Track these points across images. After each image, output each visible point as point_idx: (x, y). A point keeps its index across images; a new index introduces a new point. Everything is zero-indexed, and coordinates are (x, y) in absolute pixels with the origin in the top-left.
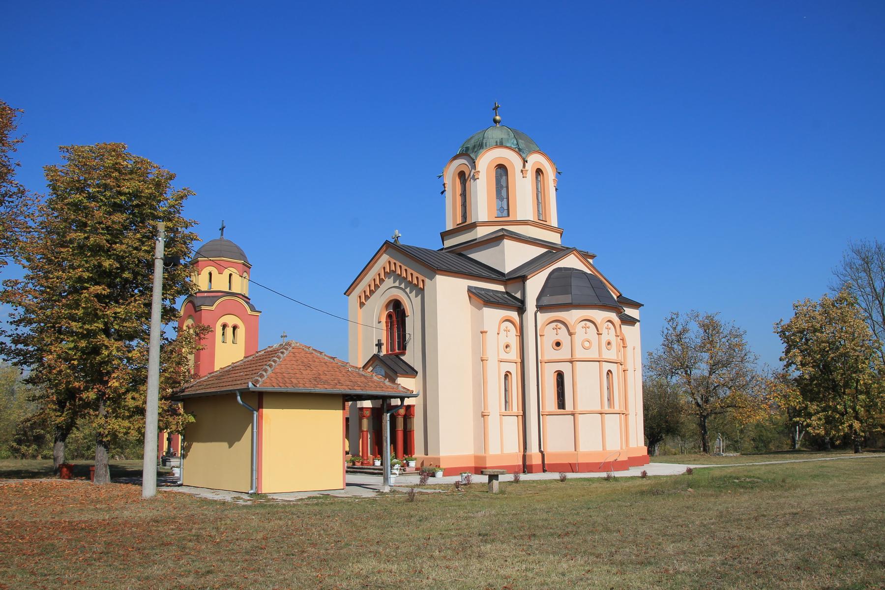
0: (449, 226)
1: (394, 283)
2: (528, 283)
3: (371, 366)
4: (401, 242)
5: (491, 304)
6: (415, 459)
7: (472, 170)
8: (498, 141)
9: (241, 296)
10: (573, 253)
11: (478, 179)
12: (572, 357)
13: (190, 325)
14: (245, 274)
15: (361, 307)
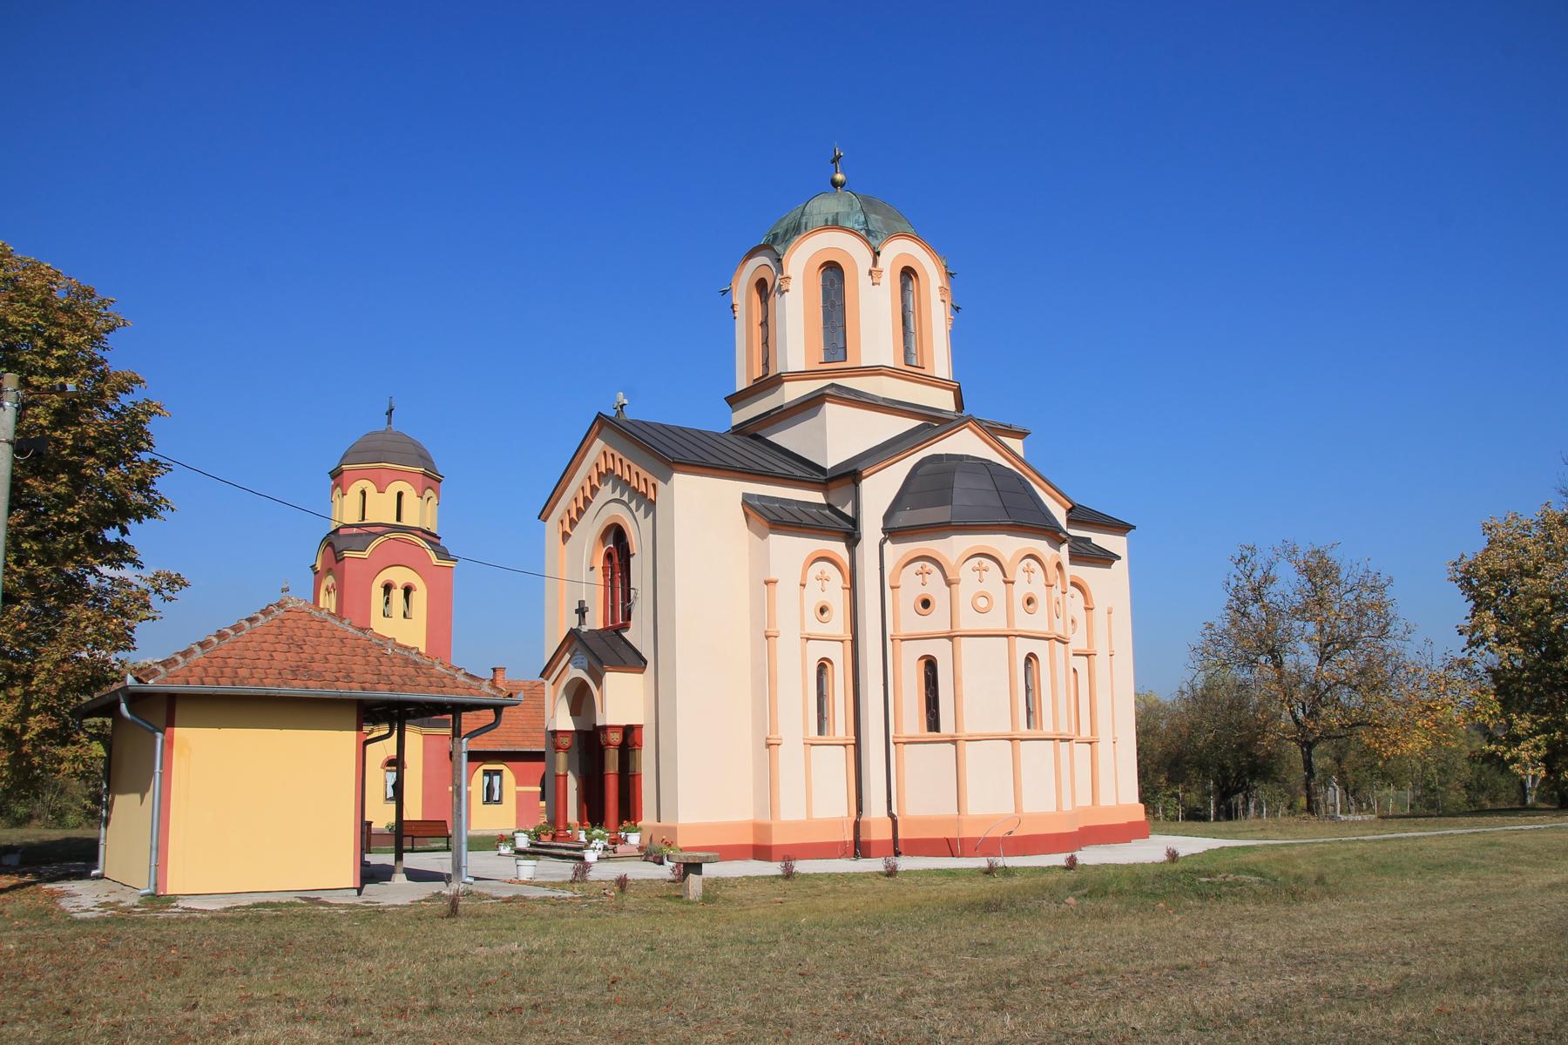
0: (742, 384)
1: (613, 492)
2: (865, 485)
3: (567, 651)
4: (629, 415)
6: (640, 829)
7: (777, 275)
8: (830, 219)
9: (419, 533)
10: (968, 427)
11: (787, 291)
13: (330, 585)
14: (429, 493)
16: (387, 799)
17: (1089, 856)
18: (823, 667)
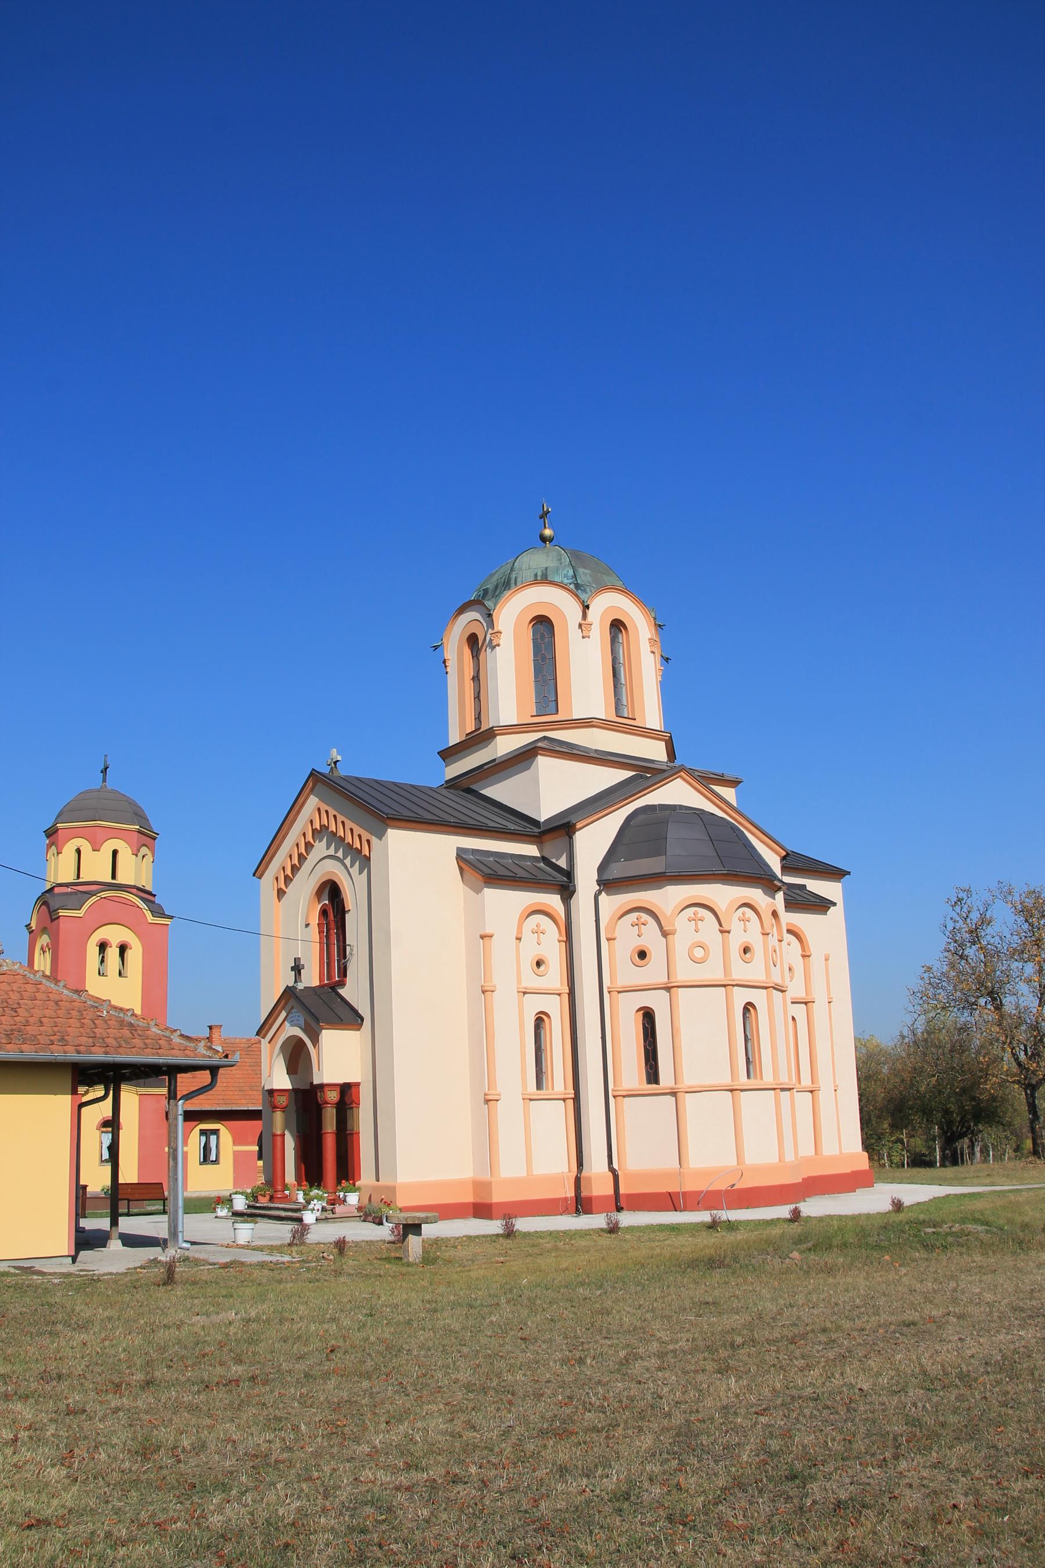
0: (455, 737)
2: (579, 837)
3: (283, 1008)
4: (343, 771)
5: (514, 884)
6: (358, 1189)
7: (488, 630)
8: (539, 574)
9: (134, 891)
10: (680, 776)
11: (498, 645)
12: (668, 979)
14: (144, 850)
15: (279, 899)
16: (102, 1161)
17: (813, 1207)
18: (540, 1021)
